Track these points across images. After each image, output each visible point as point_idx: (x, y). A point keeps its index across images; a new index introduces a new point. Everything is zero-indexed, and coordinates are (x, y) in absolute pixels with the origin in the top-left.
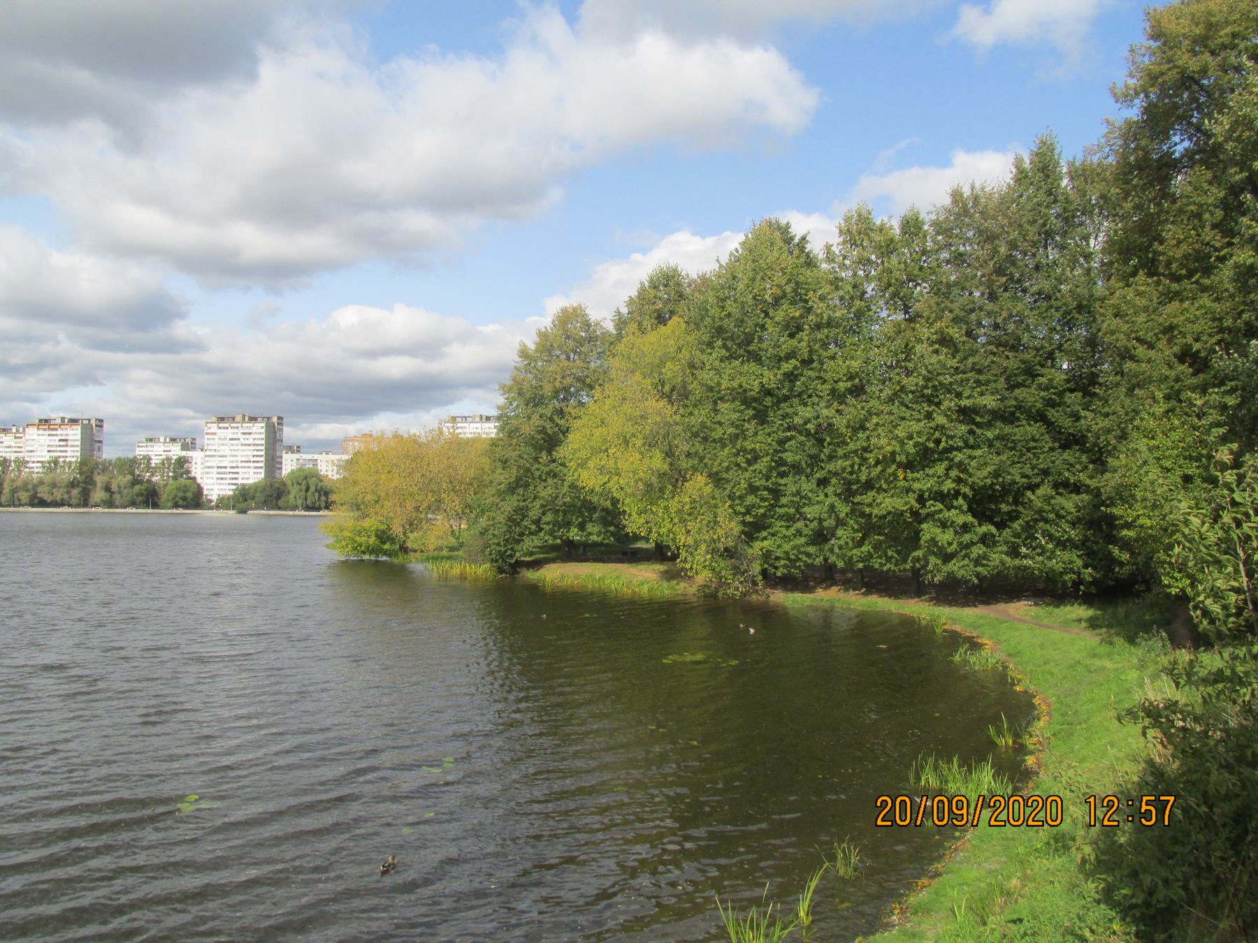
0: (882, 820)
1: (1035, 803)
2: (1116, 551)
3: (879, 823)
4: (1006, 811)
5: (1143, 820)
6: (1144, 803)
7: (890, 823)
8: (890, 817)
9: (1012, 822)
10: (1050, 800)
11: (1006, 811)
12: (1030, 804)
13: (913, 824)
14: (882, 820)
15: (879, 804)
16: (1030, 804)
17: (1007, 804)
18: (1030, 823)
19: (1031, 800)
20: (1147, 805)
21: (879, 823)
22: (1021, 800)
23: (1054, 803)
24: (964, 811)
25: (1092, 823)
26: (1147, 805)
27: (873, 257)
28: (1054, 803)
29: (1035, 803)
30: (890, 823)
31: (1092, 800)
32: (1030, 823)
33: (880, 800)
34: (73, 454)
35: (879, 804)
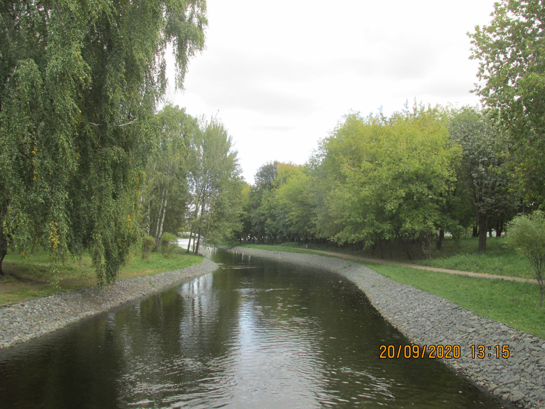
0: (382, 356)
1: (432, 349)
2: (488, 233)
3: (381, 357)
4: (436, 351)
5: (503, 356)
6: (504, 348)
7: (385, 357)
8: (386, 354)
9: (455, 356)
10: (455, 347)
11: (445, 354)
12: (446, 349)
13: (420, 357)
14: (382, 356)
15: (381, 349)
16: (446, 349)
17: (452, 349)
18: (446, 357)
19: (446, 347)
20: (505, 349)
21: (381, 357)
22: (442, 347)
23: (440, 349)
24: (418, 352)
25: (498, 357)
26: (505, 349)
27: (527, 47)
28: (440, 349)
29: (432, 349)
30: (385, 357)
31: (473, 347)
32: (446, 357)
33: (381, 347)
34: (427, 189)
35: (381, 349)
